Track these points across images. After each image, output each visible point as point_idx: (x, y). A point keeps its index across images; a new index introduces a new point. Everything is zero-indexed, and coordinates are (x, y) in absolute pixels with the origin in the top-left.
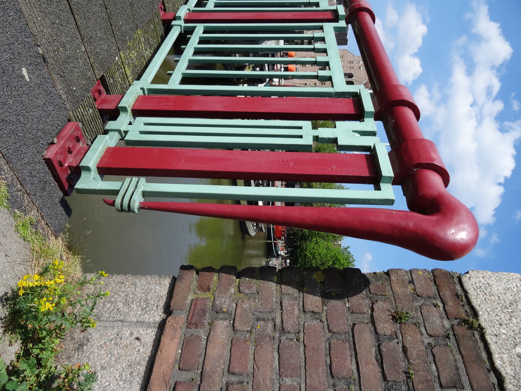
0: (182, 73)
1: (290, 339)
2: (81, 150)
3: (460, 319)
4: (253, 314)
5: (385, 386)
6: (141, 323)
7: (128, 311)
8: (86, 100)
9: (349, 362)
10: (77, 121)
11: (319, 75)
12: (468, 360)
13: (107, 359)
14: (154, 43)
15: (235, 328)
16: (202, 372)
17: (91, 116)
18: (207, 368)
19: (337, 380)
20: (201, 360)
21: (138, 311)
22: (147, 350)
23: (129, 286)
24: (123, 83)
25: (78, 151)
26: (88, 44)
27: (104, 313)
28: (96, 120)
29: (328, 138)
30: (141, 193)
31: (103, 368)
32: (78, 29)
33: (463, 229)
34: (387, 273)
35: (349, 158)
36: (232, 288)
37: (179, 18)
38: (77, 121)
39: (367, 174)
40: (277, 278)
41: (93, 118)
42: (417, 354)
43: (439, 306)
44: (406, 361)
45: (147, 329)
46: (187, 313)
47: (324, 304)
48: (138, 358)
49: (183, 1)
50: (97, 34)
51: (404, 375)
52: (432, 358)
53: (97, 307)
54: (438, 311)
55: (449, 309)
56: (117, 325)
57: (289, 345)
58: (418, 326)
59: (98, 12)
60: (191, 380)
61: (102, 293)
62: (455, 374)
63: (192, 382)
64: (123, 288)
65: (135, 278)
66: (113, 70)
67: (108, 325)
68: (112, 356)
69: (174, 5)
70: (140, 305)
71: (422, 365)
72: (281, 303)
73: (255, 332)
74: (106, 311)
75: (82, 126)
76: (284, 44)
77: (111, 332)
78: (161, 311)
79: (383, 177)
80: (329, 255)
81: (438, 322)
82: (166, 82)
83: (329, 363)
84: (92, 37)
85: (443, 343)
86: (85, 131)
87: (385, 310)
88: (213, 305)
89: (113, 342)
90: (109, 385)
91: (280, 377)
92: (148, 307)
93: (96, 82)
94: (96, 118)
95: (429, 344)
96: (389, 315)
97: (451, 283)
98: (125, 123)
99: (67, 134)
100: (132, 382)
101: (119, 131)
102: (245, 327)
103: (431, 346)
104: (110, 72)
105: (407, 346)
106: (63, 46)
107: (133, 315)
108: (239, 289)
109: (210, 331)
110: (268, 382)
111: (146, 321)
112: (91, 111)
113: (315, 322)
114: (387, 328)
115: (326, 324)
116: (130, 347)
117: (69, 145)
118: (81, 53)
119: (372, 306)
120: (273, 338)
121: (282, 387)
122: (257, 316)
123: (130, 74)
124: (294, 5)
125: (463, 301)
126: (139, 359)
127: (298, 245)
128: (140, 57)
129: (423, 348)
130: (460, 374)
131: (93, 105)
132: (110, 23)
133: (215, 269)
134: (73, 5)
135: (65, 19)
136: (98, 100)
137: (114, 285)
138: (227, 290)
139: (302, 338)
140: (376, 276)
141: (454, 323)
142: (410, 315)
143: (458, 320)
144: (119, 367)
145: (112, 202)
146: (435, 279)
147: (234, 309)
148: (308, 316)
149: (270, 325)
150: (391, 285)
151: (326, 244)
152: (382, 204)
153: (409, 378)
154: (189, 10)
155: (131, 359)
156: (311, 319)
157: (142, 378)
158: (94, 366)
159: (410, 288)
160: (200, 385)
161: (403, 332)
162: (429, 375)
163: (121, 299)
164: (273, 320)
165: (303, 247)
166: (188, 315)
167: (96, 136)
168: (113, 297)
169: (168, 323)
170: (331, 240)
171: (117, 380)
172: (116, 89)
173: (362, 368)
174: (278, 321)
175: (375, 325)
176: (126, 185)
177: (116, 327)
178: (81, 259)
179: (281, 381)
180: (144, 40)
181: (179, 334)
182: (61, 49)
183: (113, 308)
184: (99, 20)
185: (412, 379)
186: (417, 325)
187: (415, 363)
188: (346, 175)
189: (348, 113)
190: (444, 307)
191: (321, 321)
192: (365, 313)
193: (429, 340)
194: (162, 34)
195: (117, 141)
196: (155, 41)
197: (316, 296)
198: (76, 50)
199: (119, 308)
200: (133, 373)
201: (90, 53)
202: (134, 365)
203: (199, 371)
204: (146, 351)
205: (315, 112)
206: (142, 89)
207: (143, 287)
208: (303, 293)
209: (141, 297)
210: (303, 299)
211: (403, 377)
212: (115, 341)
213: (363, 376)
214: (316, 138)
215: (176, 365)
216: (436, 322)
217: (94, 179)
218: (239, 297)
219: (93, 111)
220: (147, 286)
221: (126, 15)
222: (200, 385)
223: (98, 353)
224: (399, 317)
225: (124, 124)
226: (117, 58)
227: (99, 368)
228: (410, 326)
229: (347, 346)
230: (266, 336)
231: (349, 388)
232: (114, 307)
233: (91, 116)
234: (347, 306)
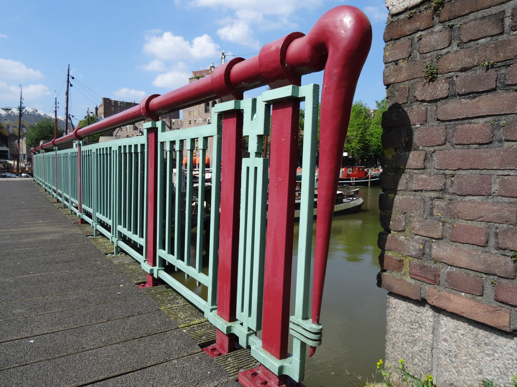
0: (199, 273)
1: (452, 184)
2: (264, 372)
3: (433, 14)
4: (426, 219)
5: (501, 90)
6: (434, 330)
7: (422, 342)
8: (220, 363)
9: (476, 126)
10: (238, 374)
11: (202, 148)
12: (475, 7)
13: (471, 367)
14: (172, 295)
15: (440, 237)
16: (485, 274)
17: (234, 360)
18: (481, 267)
19: (495, 138)
20: (472, 274)
21: (422, 332)
22: (462, 326)
23: (397, 339)
24: (206, 327)
25: (265, 375)
26: (171, 357)
27: (424, 366)
28: (238, 355)
29: (257, 144)
30: (304, 321)
31: (481, 372)
32: (159, 364)
33: (341, 21)
34: (388, 86)
35: (276, 125)
36: (400, 238)
37: (152, 270)
38: (238, 374)
39: (290, 109)
40: (391, 193)
41: (236, 358)
42: (468, 57)
43: (421, 36)
44: (476, 68)
45: (440, 324)
46: (425, 283)
47: (417, 149)
48: (470, 336)
49: (138, 265)
50: (163, 347)
51: (490, 71)
52: (472, 43)
53: (418, 371)
54: (425, 36)
55: (423, 25)
56: (437, 354)
57: (458, 185)
58: (440, 56)
59: (145, 345)
60: (494, 285)
61: (401, 367)
62: (489, 20)
63: (495, 284)
64: (398, 344)
65: (389, 332)
66: (194, 335)
67: (436, 363)
68: (468, 362)
69: (141, 274)
70: (416, 329)
71: (480, 53)
72: (415, 191)
73: (444, 218)
74: (422, 363)
75: (243, 369)
76: (176, 168)
77: (443, 360)
78: (422, 309)
79: (293, 95)
81: (436, 37)
82: (205, 288)
83: (477, 145)
84: (165, 352)
85: (457, 32)
86: (247, 366)
87: (424, 89)
88: (416, 258)
89: (454, 360)
90: (498, 368)
91: (491, 195)
92: (418, 322)
93: (204, 352)
94: (236, 356)
95: (458, 46)
96: (429, 85)
97: (398, 24)
98: (241, 329)
99: (249, 384)
100: (495, 344)
101: (248, 335)
102: (439, 227)
103: (461, 43)
104: (196, 338)
105: (460, 68)
106: (172, 379)
107: (426, 337)
108: (401, 231)
109: (442, 262)
110: (496, 208)
111: (432, 325)
112: (229, 359)
113: (435, 159)
114: (441, 88)
115: (437, 148)
116: (459, 343)
117: (259, 383)
118: (179, 363)
119: (420, 101)
120: (451, 200)
121: (501, 193)
122: (428, 215)
123: (199, 319)
124: (142, 166)
125: (416, 12)
126: (472, 335)
127: (374, 155)
128: (184, 309)
129: (462, 52)
130: (489, 15)
131: (224, 357)
132: (154, 335)
133: (381, 254)
134: (138, 366)
135: (149, 375)
136: (220, 351)
137: (396, 353)
138: (401, 243)
139: (451, 172)
140: (390, 96)
141: (438, 21)
142: (429, 64)
143: (435, 16)
144: (480, 356)
145: (312, 349)
146: (393, 39)
147: (421, 237)
148: (428, 165)
149: (437, 203)
150: (399, 83)
151: (373, 125)
152: (318, 95)
153: (492, 66)
154: (145, 261)
155: (471, 343)
156: (432, 162)
157: (491, 334)
158: (478, 381)
159: (403, 64)
160: (498, 276)
161: (446, 71)
162: (490, 45)
163: (410, 348)
164: (432, 199)
165: (376, 149)
166: (426, 283)
167: (252, 356)
168: (408, 355)
169: (434, 304)
170: (369, 120)
171: (493, 359)
172: (211, 334)
173: (482, 113)
174: (433, 195)
175: (439, 99)
176: (296, 335)
177: (438, 355)
178: (370, 382)
179: (495, 195)
180: (170, 305)
181: (445, 293)
182: (174, 381)
183: (419, 356)
184: (151, 345)
185: (494, 63)
186: (439, 58)
187: (477, 60)
188: (290, 129)
189: (236, 124)
190: (422, 31)
191: (434, 152)
192: (427, 109)
193: (454, 45)
194: (165, 287)
195: (256, 338)
196: (171, 294)
197: (408, 156)
198: (176, 368)
199: (419, 350)
200: (486, 343)
201: (179, 356)
202: (477, 341)
203: (484, 276)
204: (463, 326)
205: (234, 155)
206: (212, 310)
207: (398, 324)
208: (405, 169)
209: (408, 327)
210: (412, 169)
211: (492, 72)
212: (453, 357)
213: (491, 112)
214: (258, 154)
215: (478, 299)
216: (436, 38)
217: (290, 363)
218: (409, 232)
219: (229, 358)
220: (397, 321)
221: (148, 319)
222: (498, 276)
223: (465, 376)
224: (431, 75)
225: (242, 330)
226: (184, 331)
227: (481, 377)
228: (440, 64)
229: (459, 127)
230: (448, 208)
231: (503, 126)
232: (418, 355)
233: (234, 360)
234: (419, 126)
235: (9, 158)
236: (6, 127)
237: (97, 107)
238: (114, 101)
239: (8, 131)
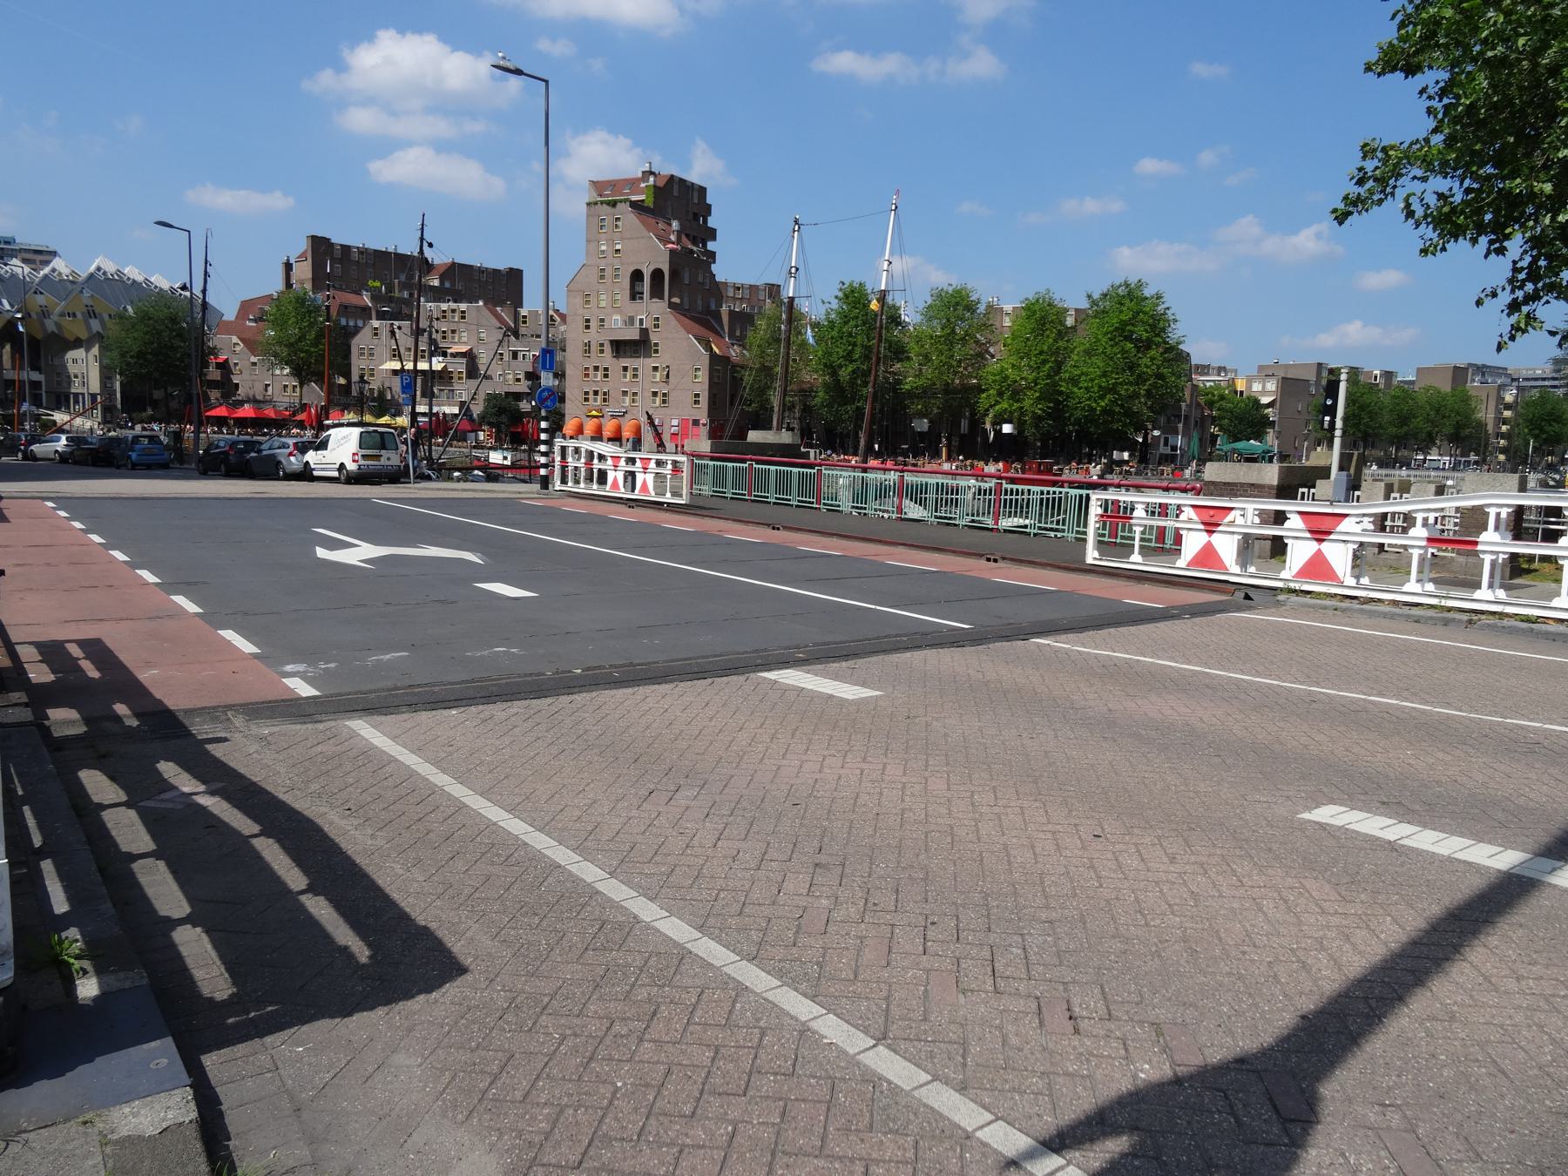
80: (1108, 351)
127: (1077, 431)
151: (1078, 355)
165: (1085, 417)
170: (1068, 341)
235: (44, 404)
236: (37, 313)
237: (288, 260)
238: (341, 245)
239: (43, 324)
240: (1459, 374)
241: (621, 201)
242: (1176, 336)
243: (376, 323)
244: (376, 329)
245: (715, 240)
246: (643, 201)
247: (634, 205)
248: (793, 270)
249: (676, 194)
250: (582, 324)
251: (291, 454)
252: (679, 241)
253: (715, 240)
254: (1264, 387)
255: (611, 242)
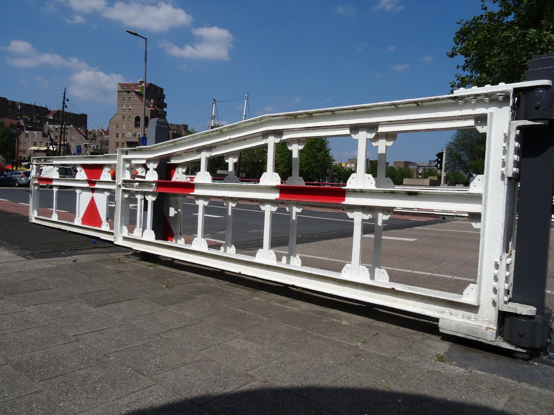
80: (308, 151)
238: (12, 101)
240: (407, 163)
241: (132, 91)
242: (329, 147)
243: (27, 132)
244: (27, 134)
245: (166, 107)
246: (140, 92)
247: (137, 93)
248: (213, 117)
249: (152, 90)
250: (115, 135)
251: (22, 177)
252: (153, 107)
253: (166, 107)
254: (351, 166)
255: (127, 106)
